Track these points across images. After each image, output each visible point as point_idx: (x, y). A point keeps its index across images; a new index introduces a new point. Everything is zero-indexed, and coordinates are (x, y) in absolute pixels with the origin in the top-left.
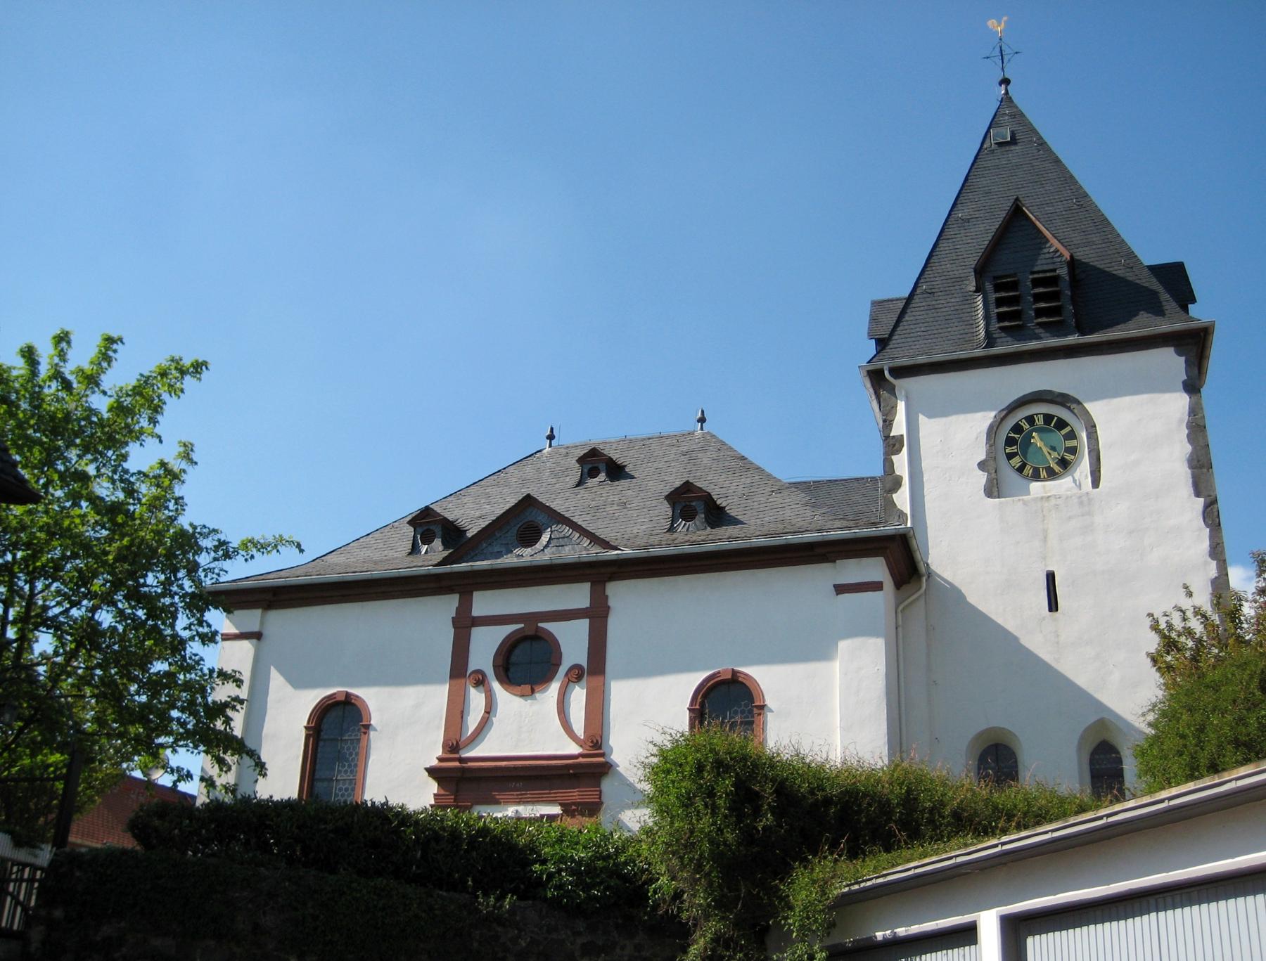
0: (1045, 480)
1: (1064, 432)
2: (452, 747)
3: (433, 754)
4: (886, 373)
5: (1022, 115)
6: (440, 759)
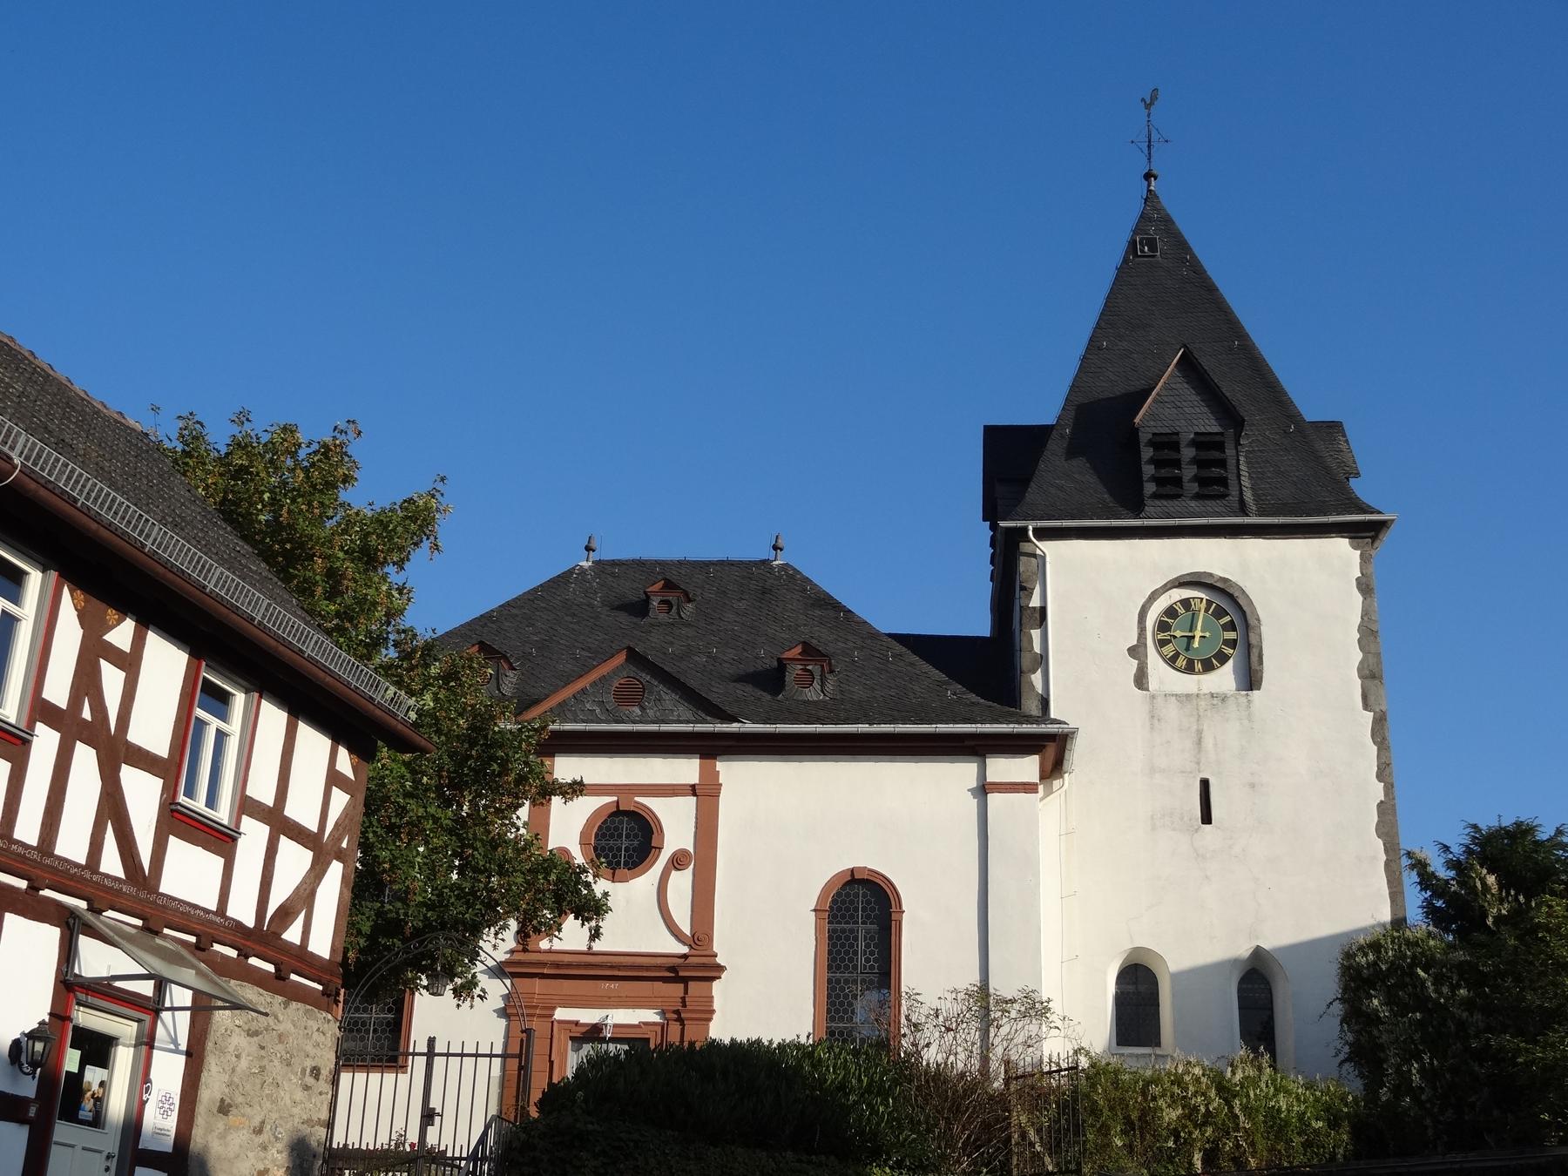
0: (1199, 673)
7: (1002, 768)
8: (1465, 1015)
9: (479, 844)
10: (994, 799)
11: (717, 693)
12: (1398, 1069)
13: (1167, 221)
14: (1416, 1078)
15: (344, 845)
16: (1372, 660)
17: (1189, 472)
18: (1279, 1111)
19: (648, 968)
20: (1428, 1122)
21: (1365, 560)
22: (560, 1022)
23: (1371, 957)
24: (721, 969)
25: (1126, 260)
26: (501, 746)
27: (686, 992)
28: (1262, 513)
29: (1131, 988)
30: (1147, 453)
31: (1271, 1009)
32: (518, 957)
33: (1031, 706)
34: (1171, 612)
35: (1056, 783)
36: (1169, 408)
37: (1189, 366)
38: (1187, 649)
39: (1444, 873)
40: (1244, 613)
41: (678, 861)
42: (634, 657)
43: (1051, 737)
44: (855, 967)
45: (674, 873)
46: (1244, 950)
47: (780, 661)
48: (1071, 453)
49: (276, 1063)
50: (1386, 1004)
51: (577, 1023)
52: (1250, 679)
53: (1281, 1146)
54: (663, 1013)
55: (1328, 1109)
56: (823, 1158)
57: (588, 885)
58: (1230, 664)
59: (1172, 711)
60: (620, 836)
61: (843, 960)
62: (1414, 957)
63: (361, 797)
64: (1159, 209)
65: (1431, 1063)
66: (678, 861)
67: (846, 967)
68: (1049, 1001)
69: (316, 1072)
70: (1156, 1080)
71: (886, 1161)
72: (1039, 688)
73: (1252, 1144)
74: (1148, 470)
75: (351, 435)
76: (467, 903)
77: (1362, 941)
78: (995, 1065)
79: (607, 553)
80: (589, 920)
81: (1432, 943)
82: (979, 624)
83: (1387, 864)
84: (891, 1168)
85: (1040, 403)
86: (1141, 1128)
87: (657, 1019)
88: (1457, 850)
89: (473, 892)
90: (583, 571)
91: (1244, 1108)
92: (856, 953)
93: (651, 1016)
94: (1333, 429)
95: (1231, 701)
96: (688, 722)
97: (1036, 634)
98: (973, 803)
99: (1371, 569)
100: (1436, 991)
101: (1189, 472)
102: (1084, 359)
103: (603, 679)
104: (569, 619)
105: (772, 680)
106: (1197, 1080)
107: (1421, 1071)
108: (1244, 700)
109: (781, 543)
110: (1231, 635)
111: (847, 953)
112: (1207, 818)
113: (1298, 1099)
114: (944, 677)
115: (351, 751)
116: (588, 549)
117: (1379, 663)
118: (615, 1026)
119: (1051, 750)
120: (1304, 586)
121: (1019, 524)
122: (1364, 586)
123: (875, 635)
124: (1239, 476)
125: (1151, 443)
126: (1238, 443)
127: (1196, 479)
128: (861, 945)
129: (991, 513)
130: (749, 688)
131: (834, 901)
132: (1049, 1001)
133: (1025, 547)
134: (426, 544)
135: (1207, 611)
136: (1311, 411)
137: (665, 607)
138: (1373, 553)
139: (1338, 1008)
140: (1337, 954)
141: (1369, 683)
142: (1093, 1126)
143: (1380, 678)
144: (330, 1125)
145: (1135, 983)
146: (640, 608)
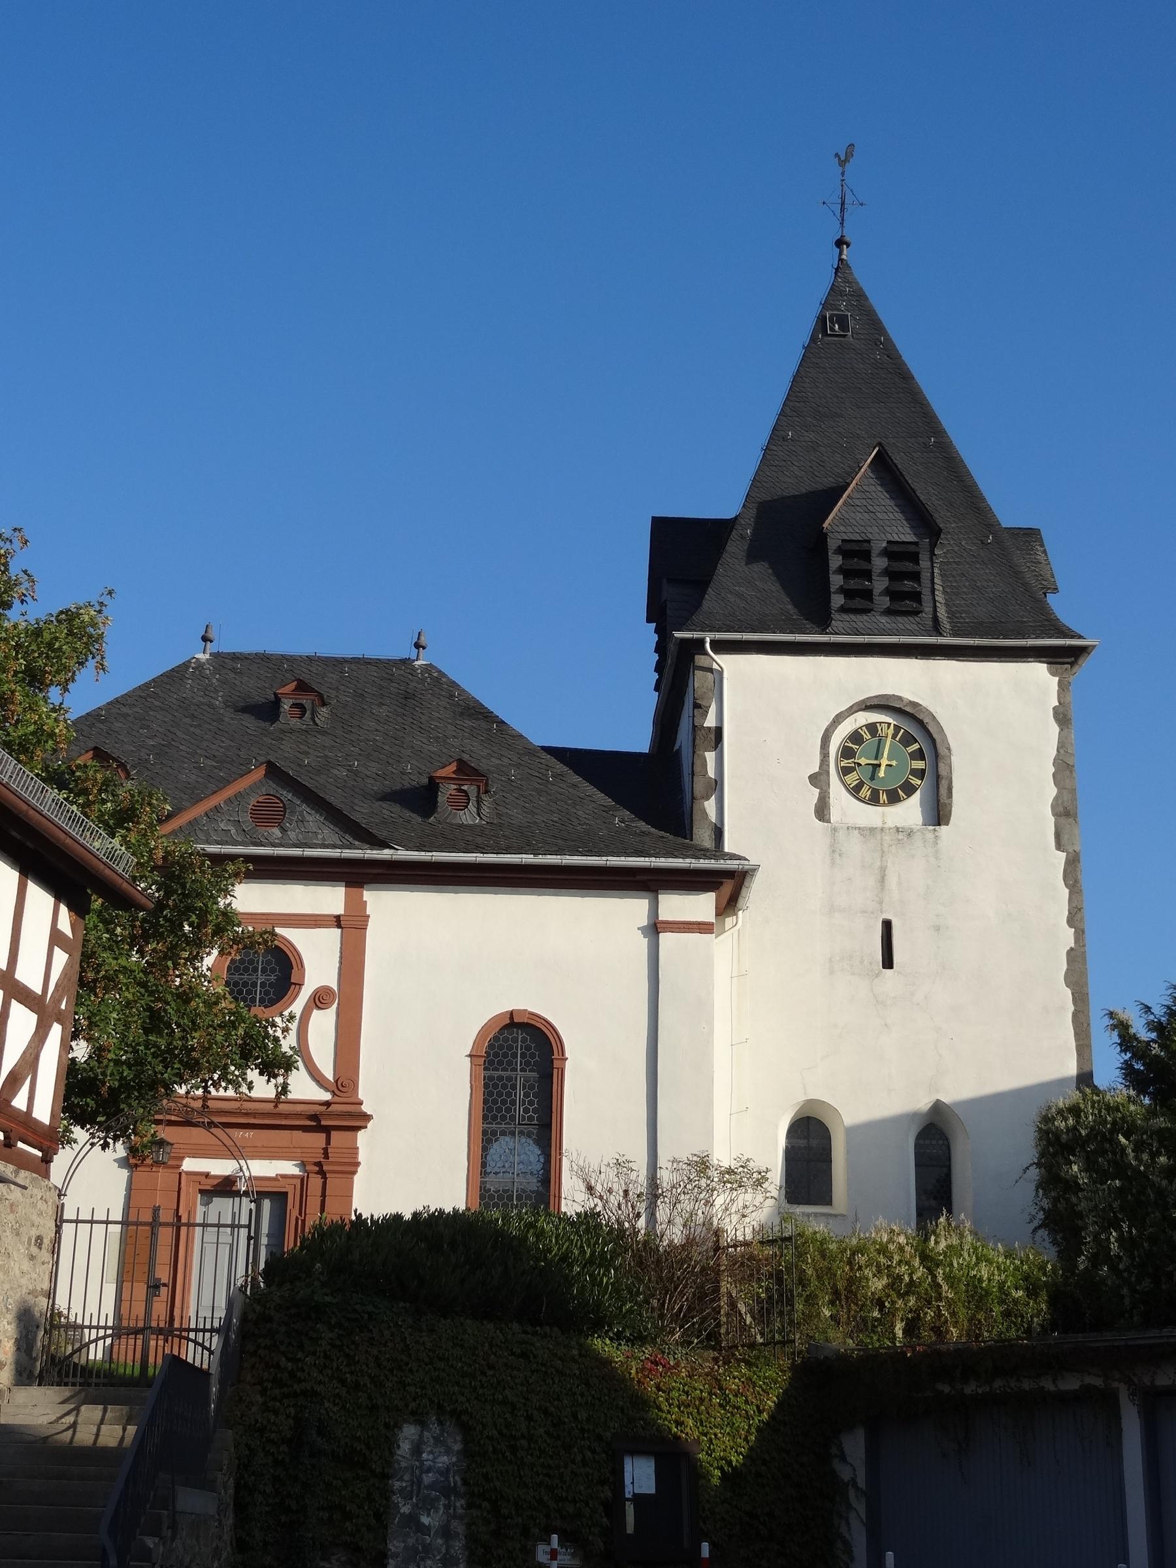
0: (884, 805)
1: (911, 749)
4: (708, 646)
5: (867, 299)
7: (674, 906)
8: (1164, 1183)
9: (169, 998)
10: (666, 939)
11: (362, 812)
12: (1096, 1237)
13: (859, 296)
14: (1114, 1247)
15: (63, 1007)
16: (1066, 796)
17: (880, 584)
18: (980, 1280)
20: (1125, 1291)
21: (1063, 687)
22: (189, 1173)
23: (1071, 1122)
24: (367, 1117)
25: (813, 339)
26: (199, 895)
27: (328, 1142)
28: (955, 634)
29: (802, 1143)
30: (835, 561)
31: (949, 1167)
33: (704, 837)
34: (856, 737)
35: (729, 921)
36: (864, 515)
37: (884, 466)
38: (872, 778)
39: (1145, 1035)
40: (933, 741)
41: (320, 999)
42: (274, 772)
43: (729, 874)
44: (513, 1118)
45: (316, 1013)
46: (923, 1103)
47: (431, 779)
48: (753, 556)
49: (8, 1233)
50: (1086, 1170)
51: (207, 1175)
52: (938, 814)
53: (981, 1316)
54: (303, 1165)
55: (1026, 1278)
56: (547, 1329)
57: (276, 1040)
58: (916, 797)
59: (854, 846)
60: (255, 970)
61: (499, 1110)
62: (1114, 1123)
63: (78, 956)
64: (851, 282)
65: (1130, 1232)
66: (320, 999)
67: (503, 1118)
68: (767, 1171)
69: (39, 1241)
70: (860, 1250)
71: (607, 1331)
72: (712, 816)
73: (953, 1314)
74: (836, 580)
75: (17, 544)
76: (164, 1061)
77: (1061, 1105)
79: (227, 643)
80: (275, 1076)
81: (1132, 1108)
82: (636, 737)
83: (1075, 1015)
84: (611, 1339)
85: (719, 491)
86: (847, 1298)
87: (296, 1171)
88: (1159, 1011)
89: (169, 1051)
90: (200, 665)
91: (947, 1278)
92: (513, 1103)
94: (1030, 536)
95: (917, 837)
96: (334, 846)
97: (710, 756)
98: (643, 943)
99: (1069, 698)
100: (1136, 1158)
101: (880, 584)
102: (767, 450)
103: (239, 796)
104: (188, 720)
105: (423, 799)
106: (901, 1249)
107: (1120, 1240)
108: (930, 836)
109: (423, 641)
110: (919, 765)
111: (504, 1102)
112: (888, 962)
113: (998, 1268)
114: (609, 802)
115: (70, 908)
116: (205, 639)
117: (1074, 799)
119: (728, 887)
120: (997, 714)
121: (696, 635)
122: (1062, 717)
123: (531, 751)
124: (933, 590)
125: (839, 551)
126: (932, 554)
127: (887, 592)
128: (520, 1093)
129: (657, 612)
130: (396, 808)
131: (491, 1046)
132: (767, 1171)
133: (700, 660)
134: (91, 663)
135: (894, 737)
136: (1009, 512)
137: (297, 711)
138: (1071, 679)
139: (1034, 1173)
140: (1032, 1116)
141: (1063, 820)
142: (800, 1295)
143: (1075, 817)
144: (51, 1294)
145: (807, 1137)
146: (269, 711)
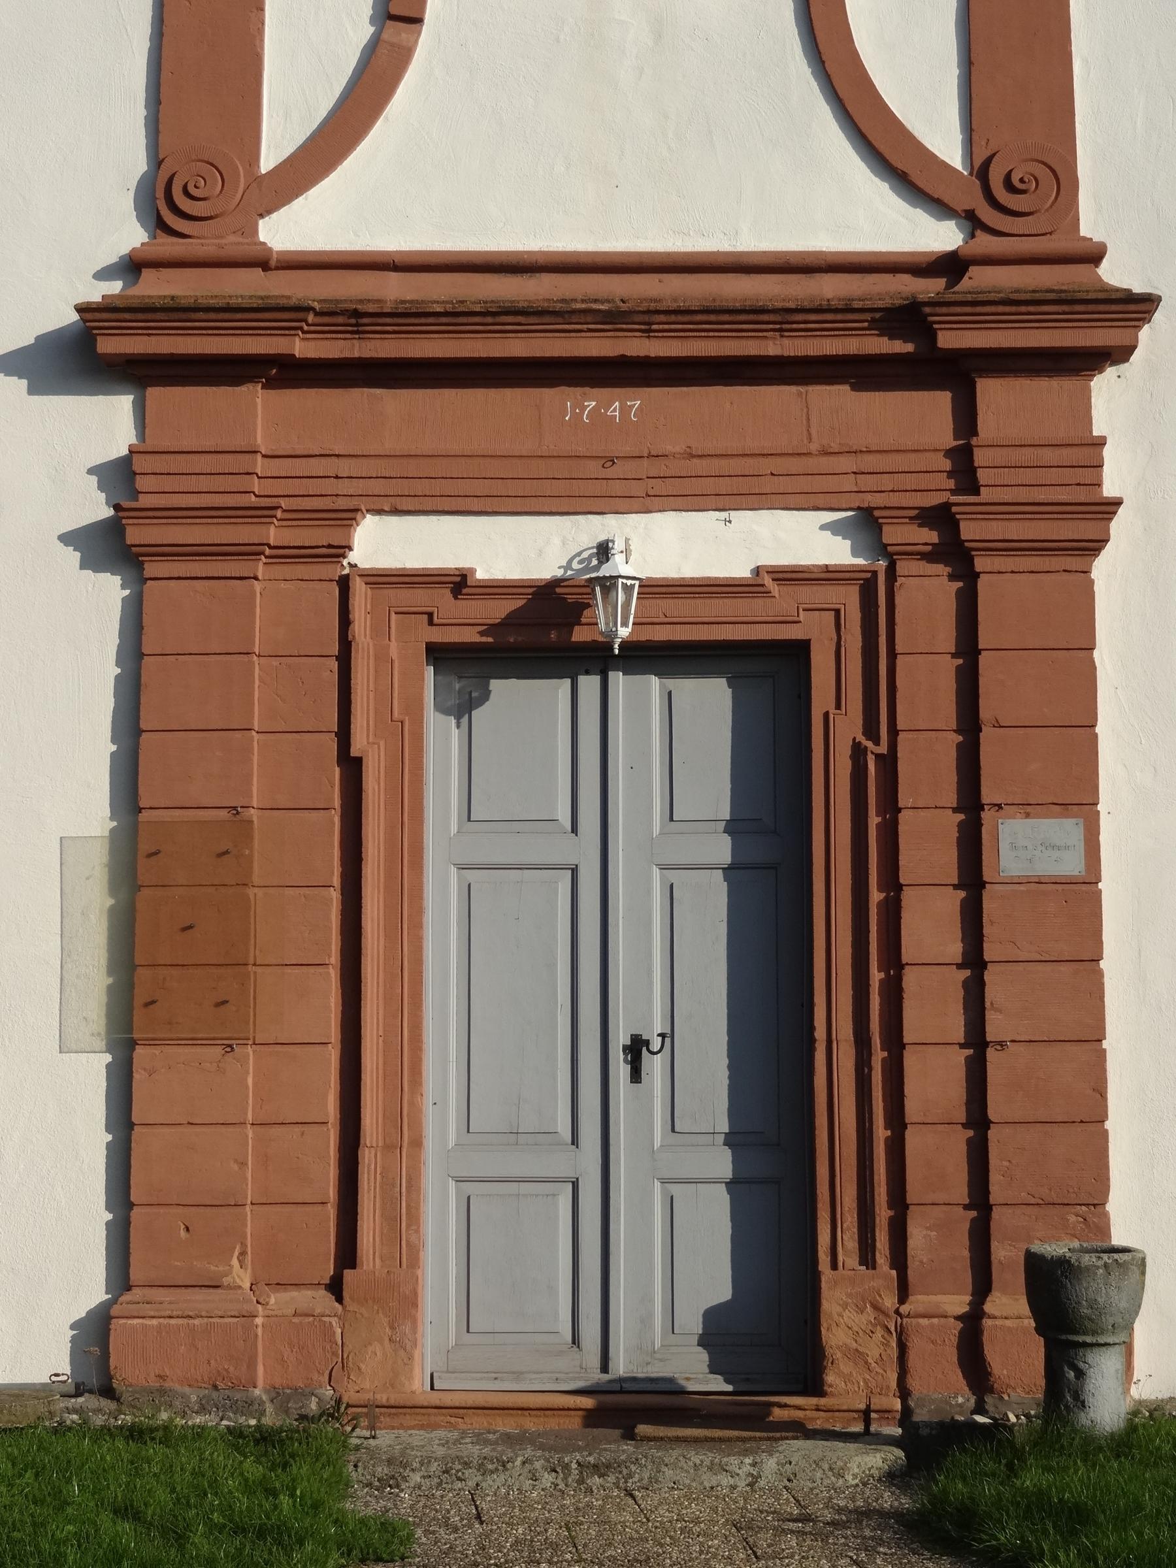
2: (197, 161)
3: (59, 226)
6: (133, 266)
19: (784, 318)
22: (380, 579)
32: (156, 286)
51: (459, 583)
54: (867, 524)
78: (888, 1500)
87: (839, 552)
93: (808, 539)
118: (652, 589)
